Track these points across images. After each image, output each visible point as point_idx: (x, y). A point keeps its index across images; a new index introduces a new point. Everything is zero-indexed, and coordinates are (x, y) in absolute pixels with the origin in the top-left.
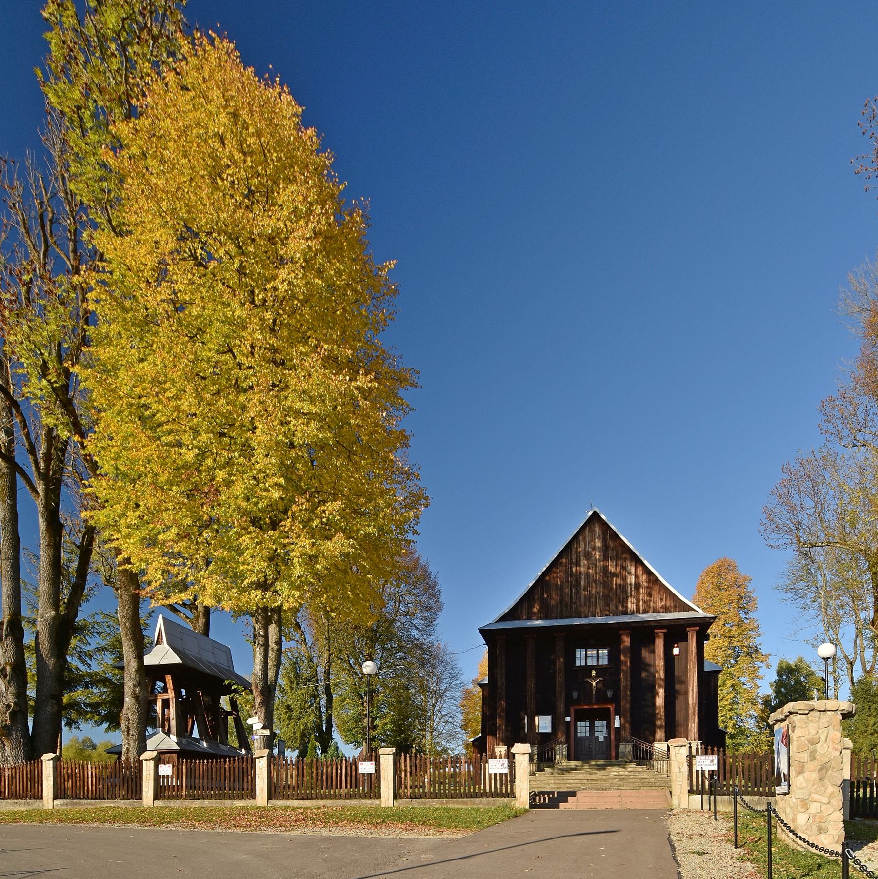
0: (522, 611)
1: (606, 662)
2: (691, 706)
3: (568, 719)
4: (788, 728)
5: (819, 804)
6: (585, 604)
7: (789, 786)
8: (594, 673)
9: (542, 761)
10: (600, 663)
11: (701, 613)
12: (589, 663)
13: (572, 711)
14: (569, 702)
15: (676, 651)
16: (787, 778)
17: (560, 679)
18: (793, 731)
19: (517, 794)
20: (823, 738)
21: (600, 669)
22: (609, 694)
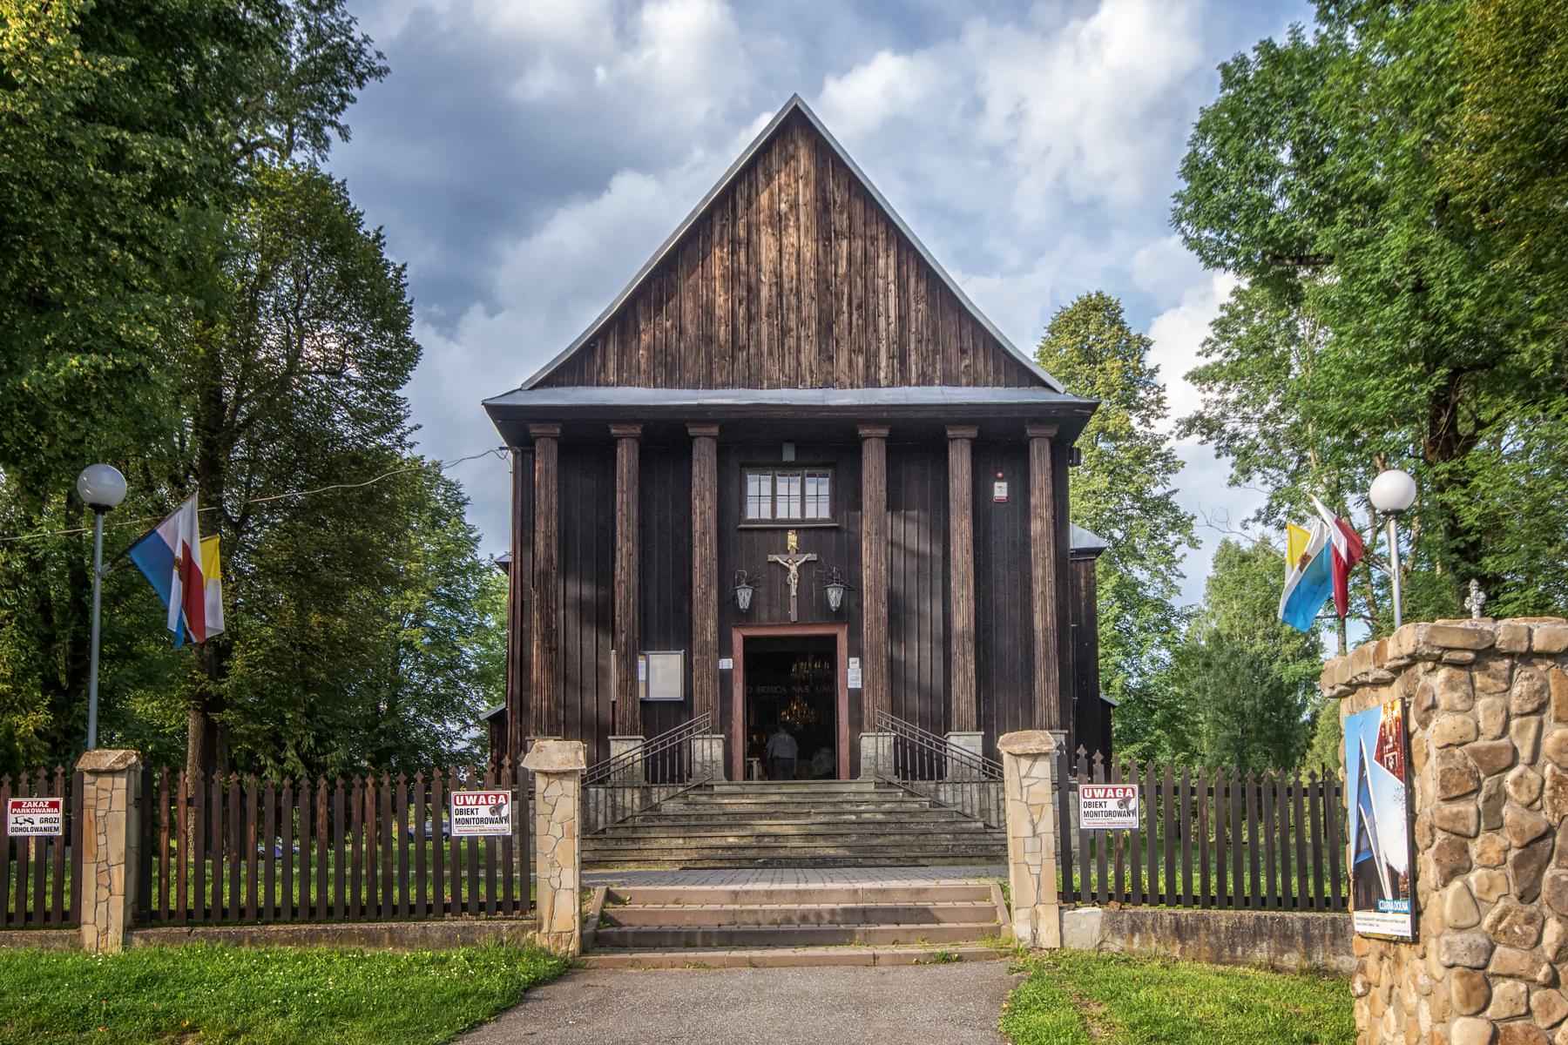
0: (604, 365)
1: (825, 513)
2: (1039, 636)
3: (726, 664)
4: (1405, 710)
5: (1522, 987)
6: (771, 353)
7: (1417, 913)
8: (792, 539)
9: (654, 781)
10: (811, 514)
11: (1064, 393)
12: (782, 514)
13: (737, 638)
14: (729, 613)
15: (1000, 490)
16: (1404, 887)
17: (704, 552)
18: (1424, 724)
19: (544, 908)
20: (1525, 753)
21: (810, 532)
22: (834, 596)
